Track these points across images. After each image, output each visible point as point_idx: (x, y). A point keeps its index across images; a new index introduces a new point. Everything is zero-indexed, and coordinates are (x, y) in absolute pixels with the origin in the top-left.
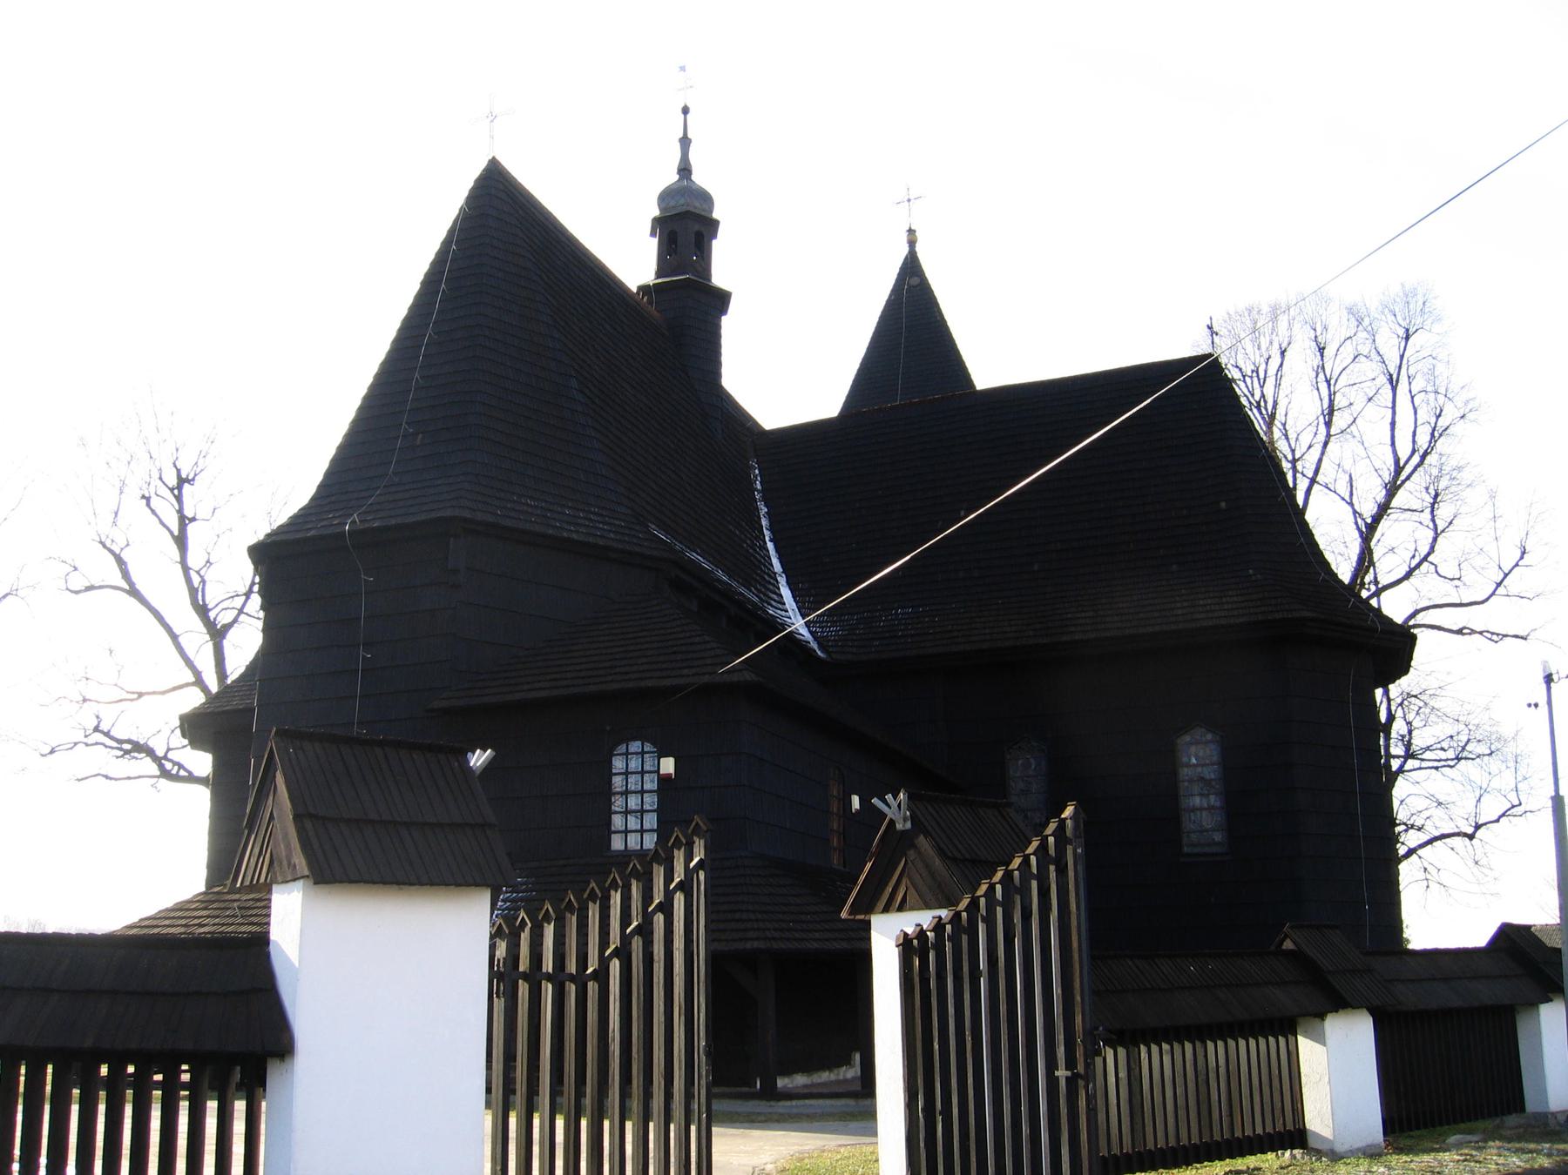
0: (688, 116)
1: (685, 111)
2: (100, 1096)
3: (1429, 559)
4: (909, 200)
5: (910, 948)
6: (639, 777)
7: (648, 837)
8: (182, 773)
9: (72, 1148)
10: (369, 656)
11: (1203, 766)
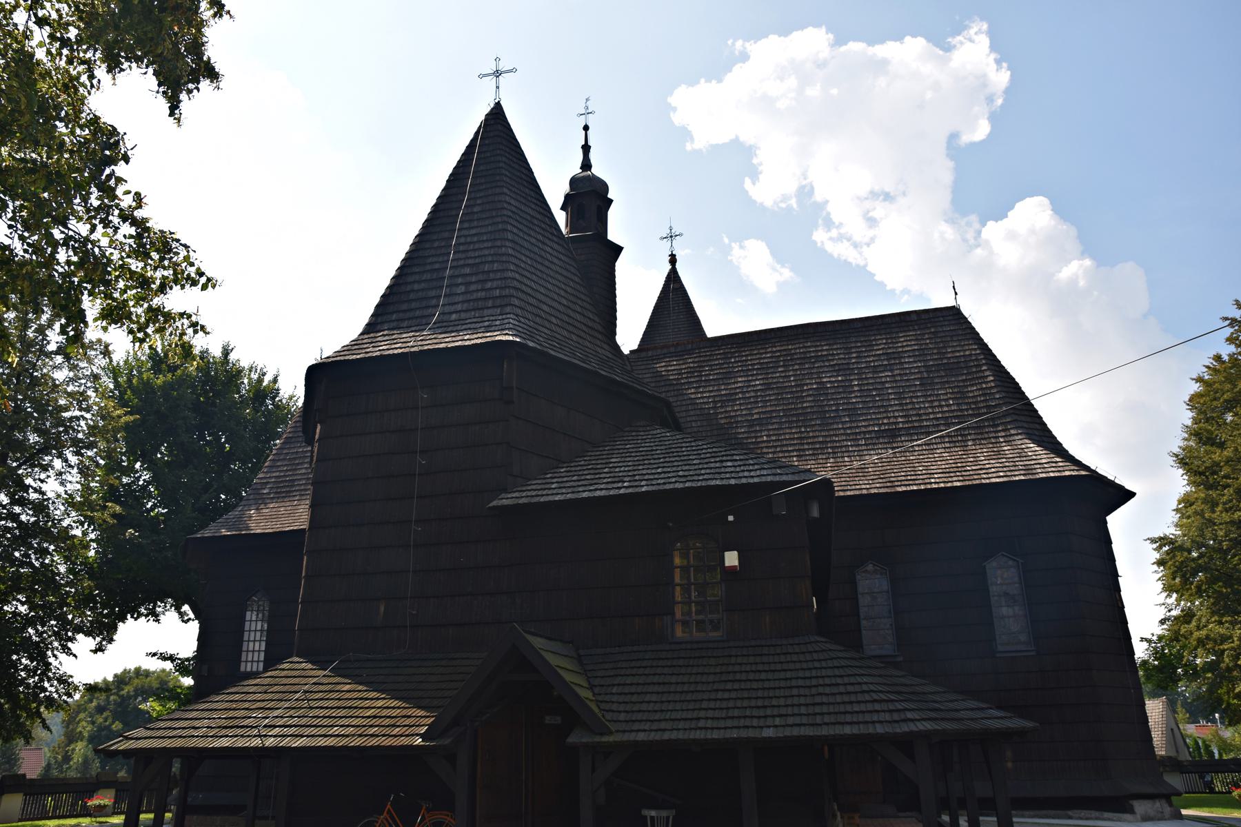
1: (586, 128)
2: (753, 736)
4: (671, 237)
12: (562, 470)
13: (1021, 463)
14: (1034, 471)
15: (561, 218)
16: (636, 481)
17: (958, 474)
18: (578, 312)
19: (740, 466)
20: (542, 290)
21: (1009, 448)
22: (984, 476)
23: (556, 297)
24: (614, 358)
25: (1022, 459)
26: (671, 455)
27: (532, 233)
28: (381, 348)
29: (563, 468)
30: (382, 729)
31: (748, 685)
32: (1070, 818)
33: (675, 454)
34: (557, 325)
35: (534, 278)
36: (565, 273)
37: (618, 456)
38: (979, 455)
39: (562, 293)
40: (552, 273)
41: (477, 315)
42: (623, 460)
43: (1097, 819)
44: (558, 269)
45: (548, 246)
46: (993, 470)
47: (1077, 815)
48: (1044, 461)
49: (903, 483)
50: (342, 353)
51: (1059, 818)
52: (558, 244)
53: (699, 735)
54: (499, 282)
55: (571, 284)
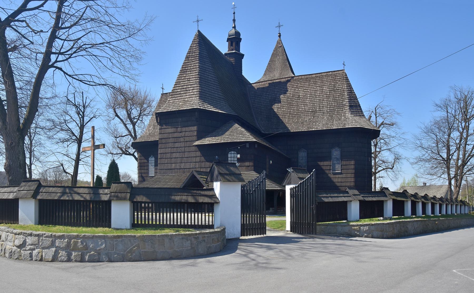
4: (279, 26)
5: (291, 189)
6: (233, 158)
8: (128, 153)
9: (190, 219)
10: (454, 271)
11: (336, 155)
20: (207, 90)
55: (216, 86)
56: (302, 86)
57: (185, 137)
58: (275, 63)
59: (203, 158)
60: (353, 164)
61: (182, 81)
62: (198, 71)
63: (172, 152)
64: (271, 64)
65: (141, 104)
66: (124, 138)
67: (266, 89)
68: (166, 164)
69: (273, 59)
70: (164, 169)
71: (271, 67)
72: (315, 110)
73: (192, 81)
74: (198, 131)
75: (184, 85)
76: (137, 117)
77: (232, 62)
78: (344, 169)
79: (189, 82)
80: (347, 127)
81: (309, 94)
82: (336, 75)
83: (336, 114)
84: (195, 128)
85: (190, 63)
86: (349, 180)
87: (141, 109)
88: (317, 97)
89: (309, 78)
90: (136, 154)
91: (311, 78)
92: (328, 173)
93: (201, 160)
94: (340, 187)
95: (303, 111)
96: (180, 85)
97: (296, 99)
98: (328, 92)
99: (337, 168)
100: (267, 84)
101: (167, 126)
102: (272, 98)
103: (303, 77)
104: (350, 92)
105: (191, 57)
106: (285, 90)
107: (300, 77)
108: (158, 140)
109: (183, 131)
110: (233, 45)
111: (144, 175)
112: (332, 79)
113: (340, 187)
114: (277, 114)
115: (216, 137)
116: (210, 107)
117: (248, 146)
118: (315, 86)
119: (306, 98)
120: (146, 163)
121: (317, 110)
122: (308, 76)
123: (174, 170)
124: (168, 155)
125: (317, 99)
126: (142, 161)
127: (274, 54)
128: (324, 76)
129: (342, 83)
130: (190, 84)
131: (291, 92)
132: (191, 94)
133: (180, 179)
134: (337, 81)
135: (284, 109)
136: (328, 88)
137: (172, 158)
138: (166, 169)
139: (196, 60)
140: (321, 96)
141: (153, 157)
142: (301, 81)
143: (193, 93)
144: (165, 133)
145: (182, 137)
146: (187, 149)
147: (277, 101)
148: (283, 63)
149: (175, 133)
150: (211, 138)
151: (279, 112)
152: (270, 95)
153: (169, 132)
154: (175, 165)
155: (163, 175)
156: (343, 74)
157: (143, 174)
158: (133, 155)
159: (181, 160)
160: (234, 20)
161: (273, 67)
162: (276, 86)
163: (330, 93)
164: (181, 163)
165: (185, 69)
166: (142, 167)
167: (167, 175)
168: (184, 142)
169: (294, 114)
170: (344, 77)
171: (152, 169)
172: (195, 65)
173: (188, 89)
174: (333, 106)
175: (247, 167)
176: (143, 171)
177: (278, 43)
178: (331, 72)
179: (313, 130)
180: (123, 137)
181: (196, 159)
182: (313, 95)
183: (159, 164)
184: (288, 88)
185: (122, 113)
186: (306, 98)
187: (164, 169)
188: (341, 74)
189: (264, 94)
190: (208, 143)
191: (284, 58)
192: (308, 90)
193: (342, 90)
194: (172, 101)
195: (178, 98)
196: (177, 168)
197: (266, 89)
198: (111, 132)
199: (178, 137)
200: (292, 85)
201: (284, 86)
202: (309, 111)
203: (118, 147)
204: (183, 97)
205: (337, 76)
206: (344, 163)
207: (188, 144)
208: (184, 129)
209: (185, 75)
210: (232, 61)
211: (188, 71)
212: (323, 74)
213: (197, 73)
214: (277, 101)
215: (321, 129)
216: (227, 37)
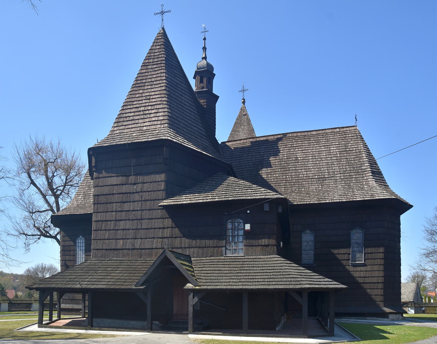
0: (204, 46)
3: (32, 185)
4: (243, 91)
7: (240, 244)
8: (48, 234)
12: (187, 192)
13: (370, 193)
14: (374, 196)
15: (193, 83)
16: (214, 196)
17: (345, 196)
18: (195, 127)
19: (253, 192)
20: (181, 117)
21: (367, 186)
22: (355, 198)
23: (186, 120)
24: (210, 146)
25: (371, 191)
26: (228, 186)
27: (177, 91)
28: (116, 141)
29: (187, 191)
30: (121, 283)
31: (249, 271)
32: (366, 319)
33: (230, 186)
34: (187, 132)
35: (177, 111)
36: (191, 109)
37: (209, 186)
38: (354, 189)
39: (189, 118)
40: (185, 109)
41: (154, 128)
42: (210, 188)
43: (375, 320)
44: (187, 107)
45: (183, 97)
46: (359, 195)
47: (369, 319)
48: (379, 192)
49: (323, 199)
50: (101, 143)
51: (362, 319)
52: (188, 96)
53: (229, 287)
54: (163, 113)
55: (193, 114)
56: (300, 145)
57: (143, 192)
58: (239, 134)
59: (177, 231)
60: (382, 252)
61: (136, 99)
62: (165, 84)
63: (118, 218)
64: (233, 134)
65: (67, 171)
66: (43, 213)
67: (247, 149)
68: (105, 241)
69: (236, 128)
70: (103, 249)
71: (234, 138)
72: (322, 176)
73: (154, 100)
74: (167, 182)
75: (140, 105)
76: (61, 188)
77: (203, 104)
78: (368, 259)
79: (148, 101)
80: (377, 198)
81: (311, 155)
82: (345, 132)
83: (354, 181)
84: (162, 177)
85: (150, 74)
86: (376, 274)
87: (67, 177)
88: (323, 159)
89: (307, 136)
90: (59, 237)
91: (311, 136)
92: (345, 265)
93: (172, 235)
94: (362, 285)
95: (305, 178)
96: (132, 107)
97: (292, 161)
98: (338, 153)
99: (358, 258)
100: (248, 143)
101: (108, 173)
102: (257, 161)
103: (299, 134)
104: (368, 154)
105: (151, 64)
106: (275, 150)
107: (295, 135)
108: (92, 214)
109: (138, 182)
110: (204, 82)
111: (69, 263)
112: (340, 137)
113: (362, 285)
114: (268, 181)
115: (202, 194)
116: (188, 143)
117: (266, 208)
118: (318, 145)
119: (307, 161)
120: (72, 247)
121: (326, 176)
122: (306, 133)
123: (121, 251)
124: (111, 225)
125: (324, 162)
126: (67, 244)
127: (237, 123)
128: (329, 134)
129: (356, 142)
130: (150, 104)
131: (284, 153)
132: (154, 119)
133: (134, 267)
134: (349, 140)
135: (277, 175)
136: (338, 148)
137: (118, 230)
138: (106, 249)
139: (161, 68)
140: (329, 159)
141: (83, 238)
142: (296, 139)
143: (156, 119)
144: (106, 186)
145: (137, 192)
146: (146, 214)
147: (265, 165)
148: (248, 134)
149: (123, 185)
150: (192, 195)
151: (270, 178)
152: (254, 157)
153: (113, 184)
154: (123, 243)
155: (101, 259)
156: (355, 131)
157: (67, 261)
158: (55, 237)
159: (134, 233)
160: (205, 49)
161: (236, 138)
162: (261, 145)
163: (341, 155)
164: (136, 239)
165: (141, 81)
166: (67, 252)
167: (108, 259)
168: (141, 201)
169: (292, 181)
170: (358, 134)
171: (82, 255)
172: (159, 75)
173: (147, 112)
174: (348, 172)
175: (265, 247)
176: (67, 258)
177: (242, 110)
178: (339, 128)
179: (328, 201)
180: (41, 212)
181: (163, 233)
182: (317, 157)
183: (93, 240)
184: (280, 147)
185: (41, 181)
186: (307, 161)
187: (103, 249)
188: (353, 131)
189: (246, 155)
190: (188, 202)
191: (249, 128)
192: (309, 151)
193: (358, 151)
194: (118, 132)
195: (130, 126)
196: (127, 248)
197: (247, 149)
198: (25, 206)
199: (130, 193)
200: (285, 144)
201: (273, 146)
202: (313, 177)
203: (34, 226)
204: (139, 125)
205: (347, 133)
206: (369, 250)
207: (148, 205)
208: (140, 179)
209: (141, 91)
210: (203, 103)
211: (146, 85)
212: (327, 131)
213: (163, 87)
214: (265, 165)
215: (338, 201)
216: (195, 69)
